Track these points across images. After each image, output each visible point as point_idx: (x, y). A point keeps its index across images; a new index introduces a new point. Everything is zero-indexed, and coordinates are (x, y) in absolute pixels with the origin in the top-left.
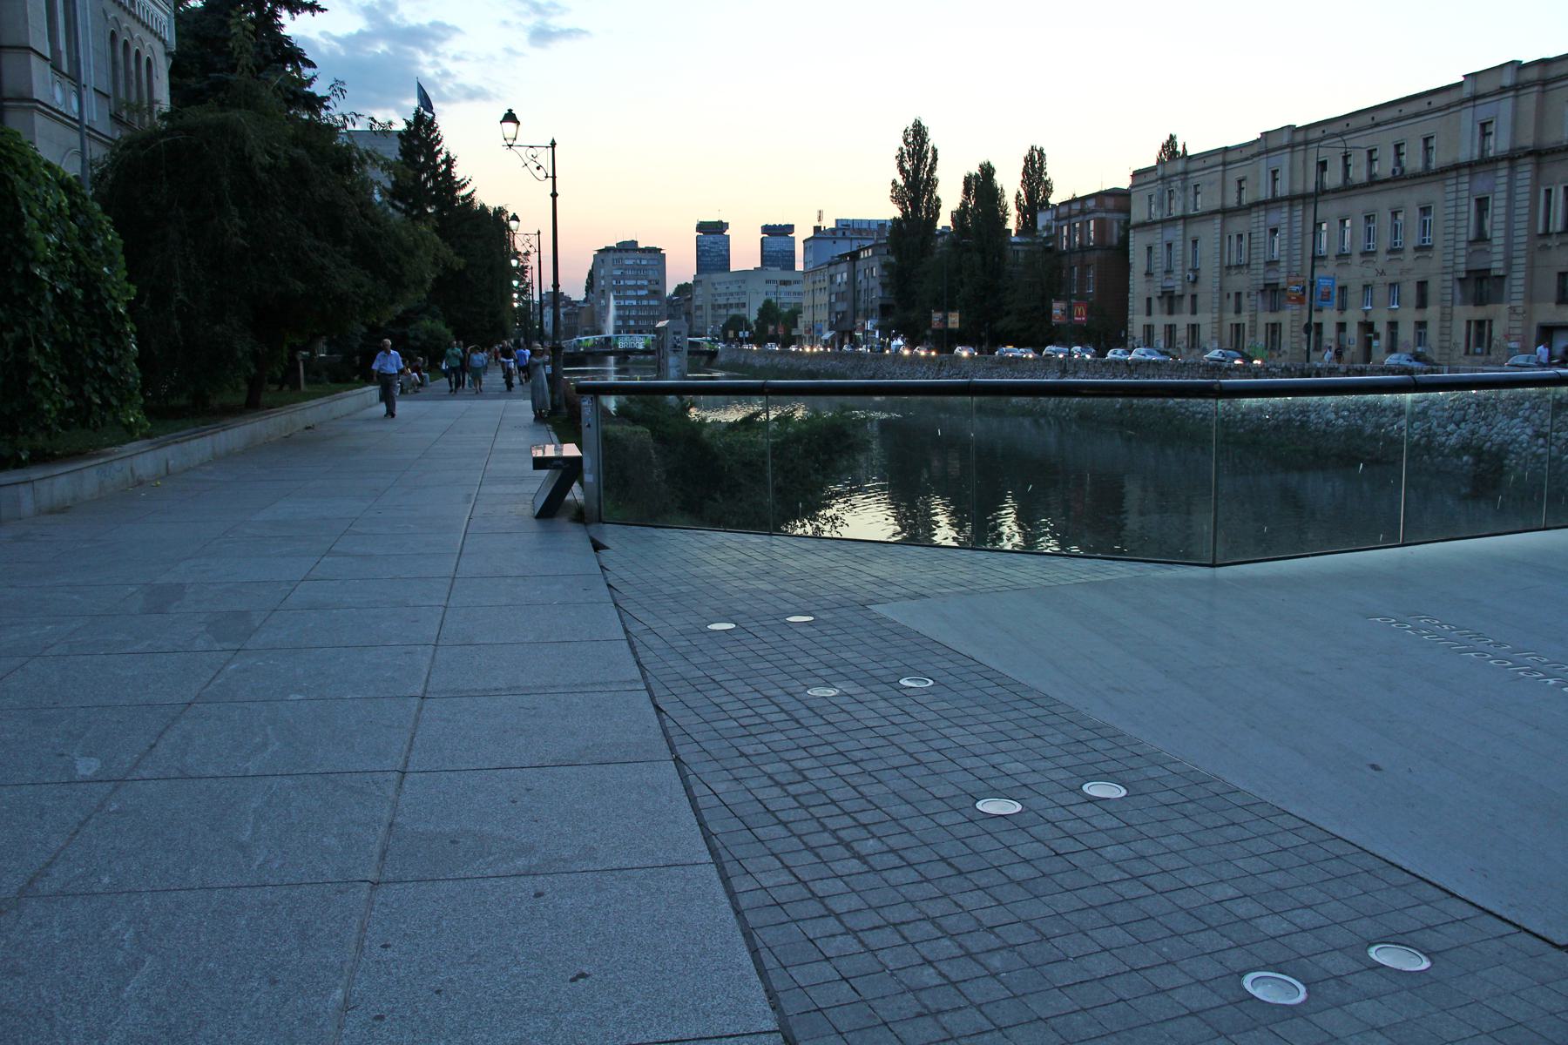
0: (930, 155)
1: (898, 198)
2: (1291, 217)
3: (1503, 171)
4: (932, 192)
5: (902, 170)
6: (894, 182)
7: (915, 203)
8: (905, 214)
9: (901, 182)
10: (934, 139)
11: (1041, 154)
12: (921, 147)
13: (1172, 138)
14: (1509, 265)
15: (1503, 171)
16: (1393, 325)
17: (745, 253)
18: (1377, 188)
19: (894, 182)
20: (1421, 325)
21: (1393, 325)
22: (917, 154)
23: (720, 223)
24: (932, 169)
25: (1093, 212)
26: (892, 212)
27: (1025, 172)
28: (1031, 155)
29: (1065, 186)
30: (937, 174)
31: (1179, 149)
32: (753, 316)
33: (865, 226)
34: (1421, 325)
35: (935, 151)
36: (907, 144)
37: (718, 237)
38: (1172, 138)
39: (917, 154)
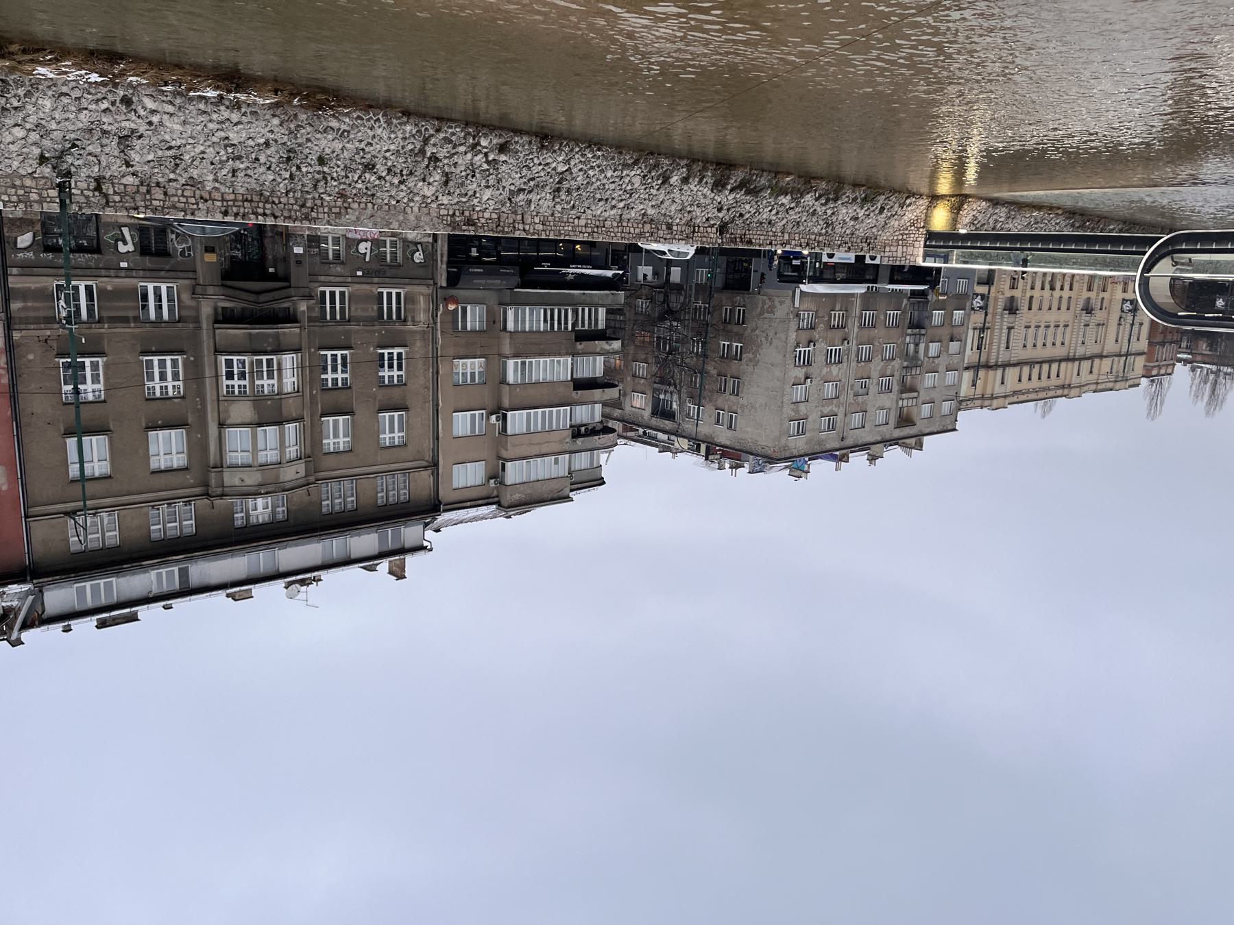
14: (1002, 315)
20: (1032, 288)
34: (1032, 288)
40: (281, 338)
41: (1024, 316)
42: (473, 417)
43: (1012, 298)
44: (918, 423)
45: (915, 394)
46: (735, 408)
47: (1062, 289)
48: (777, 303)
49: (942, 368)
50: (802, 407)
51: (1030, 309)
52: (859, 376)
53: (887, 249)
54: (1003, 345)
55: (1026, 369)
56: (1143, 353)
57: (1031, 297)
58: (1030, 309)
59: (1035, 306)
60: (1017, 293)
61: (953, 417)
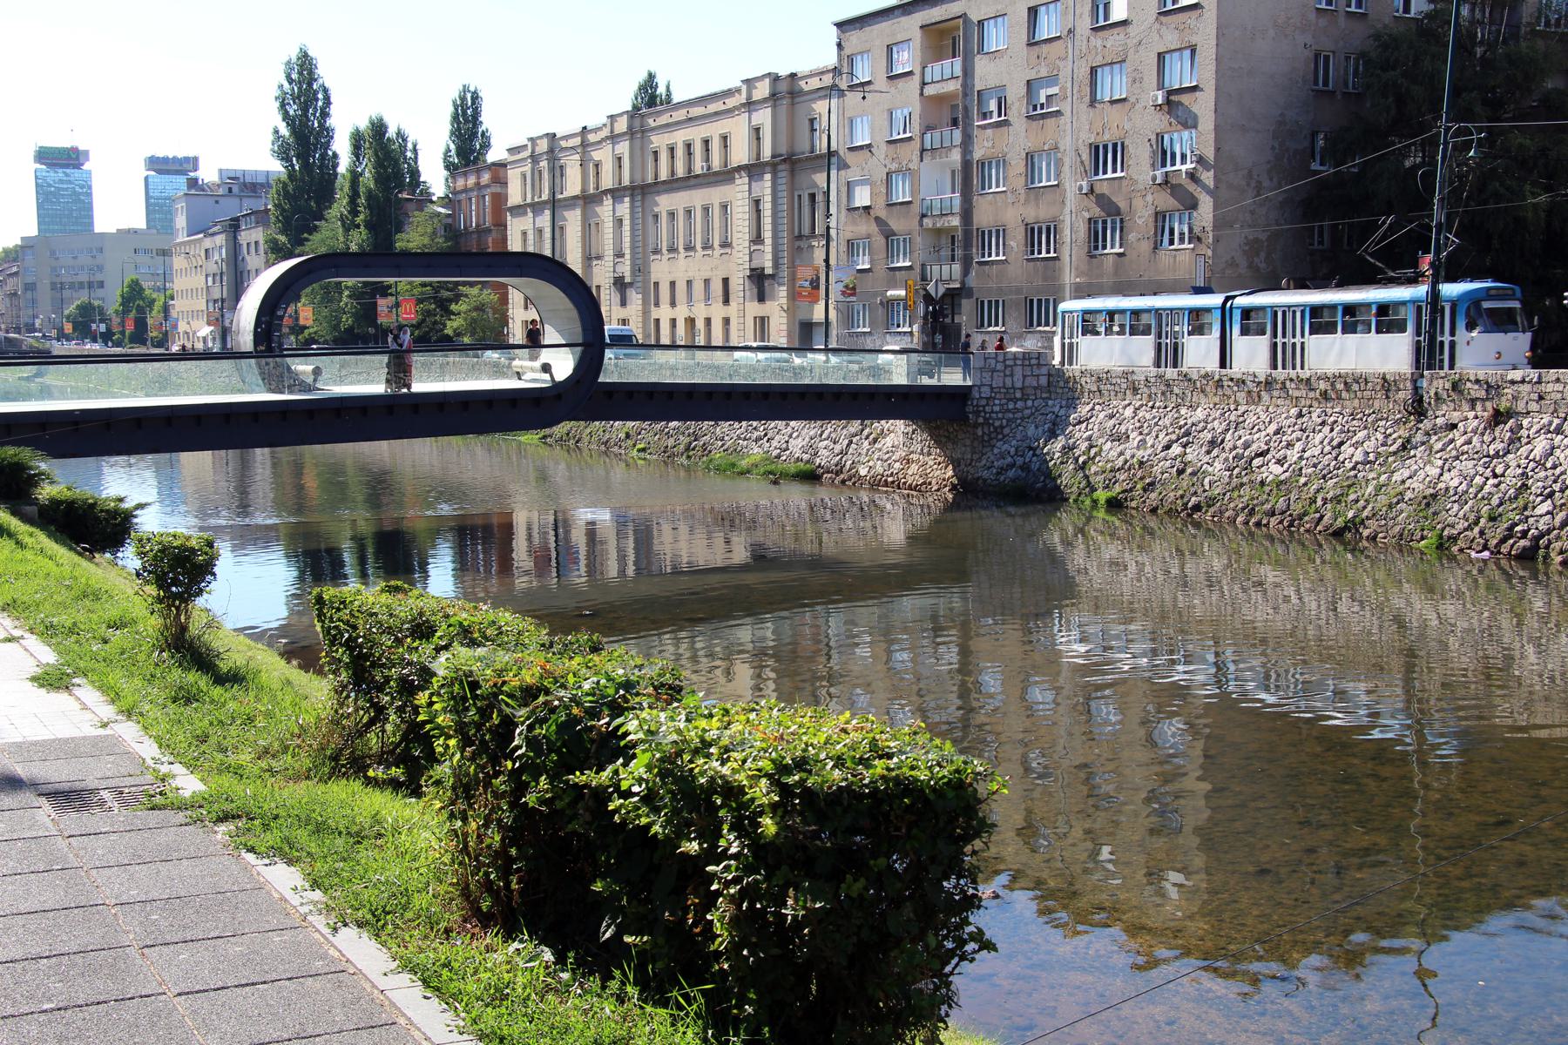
0: (320, 96)
1: (283, 153)
2: (632, 208)
3: (742, 181)
4: (327, 146)
5: (286, 117)
6: (276, 132)
7: (303, 156)
8: (291, 175)
9: (284, 131)
10: (326, 74)
11: (476, 97)
12: (310, 85)
13: (651, 76)
14: (776, 265)
15: (742, 181)
16: (708, 321)
17: (118, 207)
18: (693, 182)
19: (276, 132)
20: (727, 321)
21: (708, 321)
22: (305, 98)
23: (75, 150)
24: (325, 115)
25: (487, 186)
26: (276, 167)
27: (455, 118)
28: (463, 99)
29: (504, 134)
30: (330, 122)
31: (661, 90)
32: (112, 305)
33: (261, 180)
34: (727, 321)
35: (326, 90)
36: (290, 81)
37: (75, 173)
38: (651, 76)
39: (305, 98)
40: (235, 379)
41: (737, 268)
42: (1106, 18)
43: (761, 298)
44: (917, 35)
45: (929, 91)
46: (1323, 22)
47: (673, 322)
48: (1243, 263)
49: (881, 150)
50: (1171, 40)
51: (726, 281)
52: (1050, 122)
53: (1043, 381)
54: (627, 223)
55: (699, 167)
56: (511, 209)
57: (726, 301)
58: (726, 281)
59: (717, 287)
60: (754, 309)
61: (847, 51)
